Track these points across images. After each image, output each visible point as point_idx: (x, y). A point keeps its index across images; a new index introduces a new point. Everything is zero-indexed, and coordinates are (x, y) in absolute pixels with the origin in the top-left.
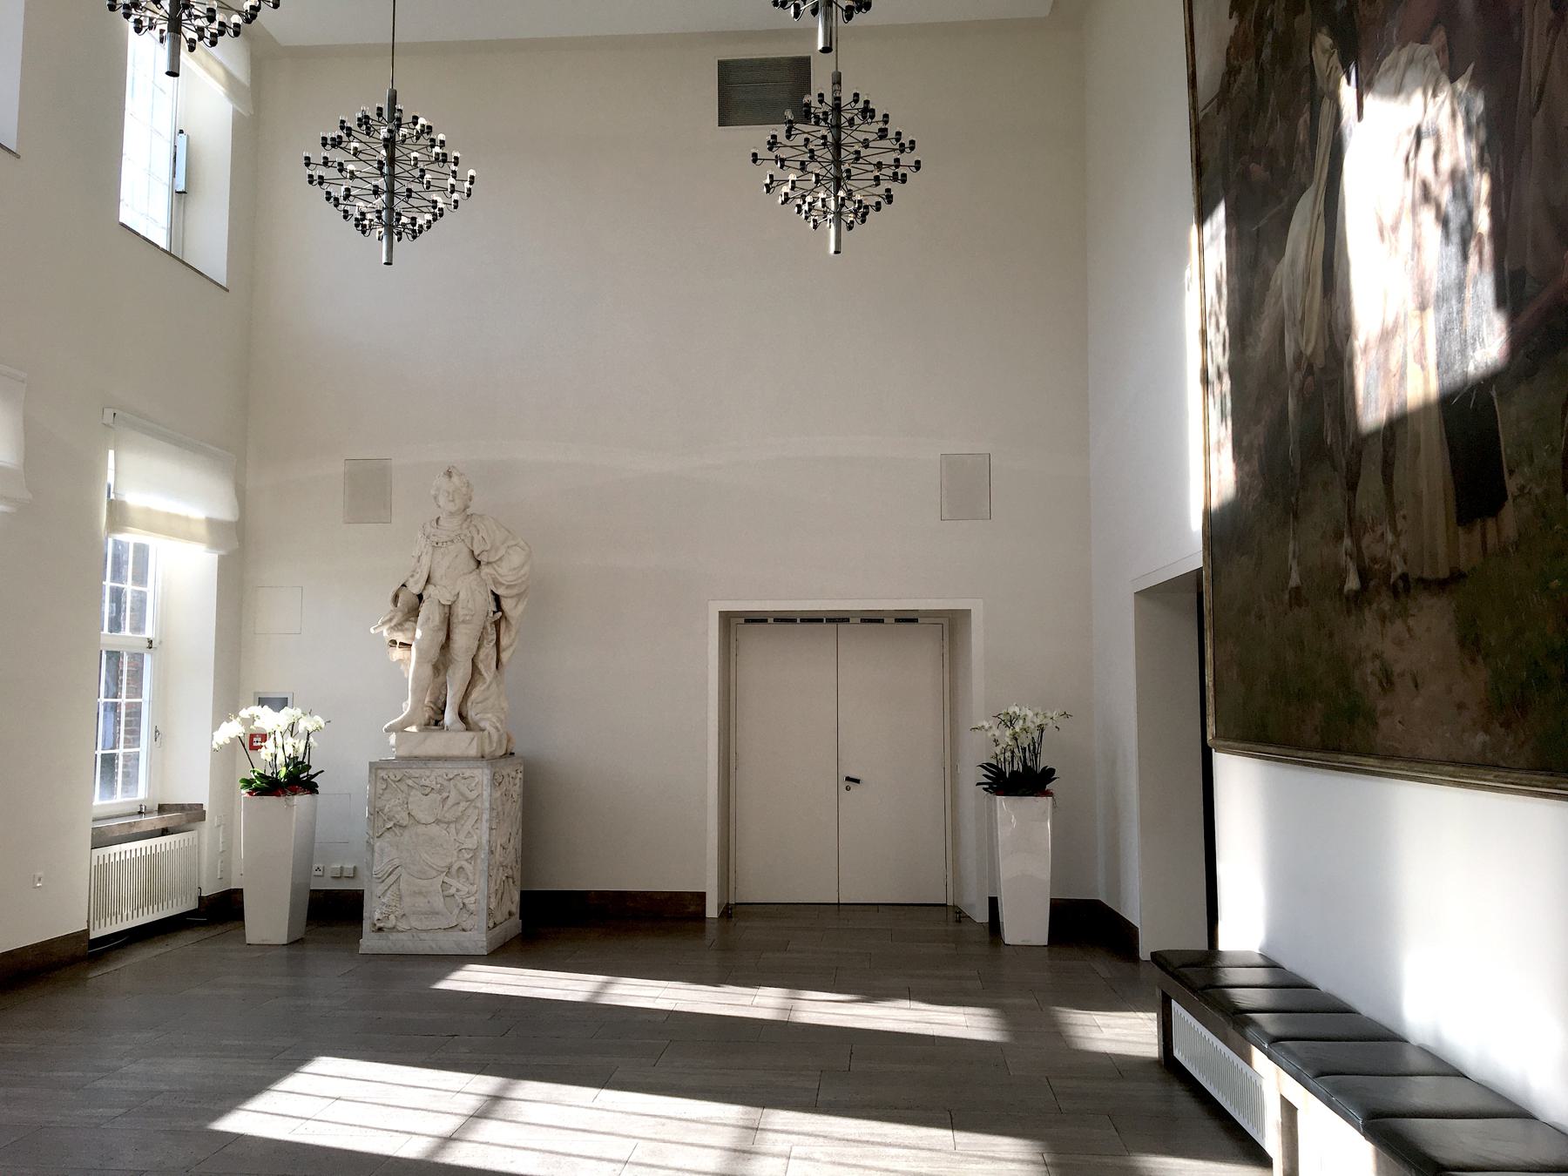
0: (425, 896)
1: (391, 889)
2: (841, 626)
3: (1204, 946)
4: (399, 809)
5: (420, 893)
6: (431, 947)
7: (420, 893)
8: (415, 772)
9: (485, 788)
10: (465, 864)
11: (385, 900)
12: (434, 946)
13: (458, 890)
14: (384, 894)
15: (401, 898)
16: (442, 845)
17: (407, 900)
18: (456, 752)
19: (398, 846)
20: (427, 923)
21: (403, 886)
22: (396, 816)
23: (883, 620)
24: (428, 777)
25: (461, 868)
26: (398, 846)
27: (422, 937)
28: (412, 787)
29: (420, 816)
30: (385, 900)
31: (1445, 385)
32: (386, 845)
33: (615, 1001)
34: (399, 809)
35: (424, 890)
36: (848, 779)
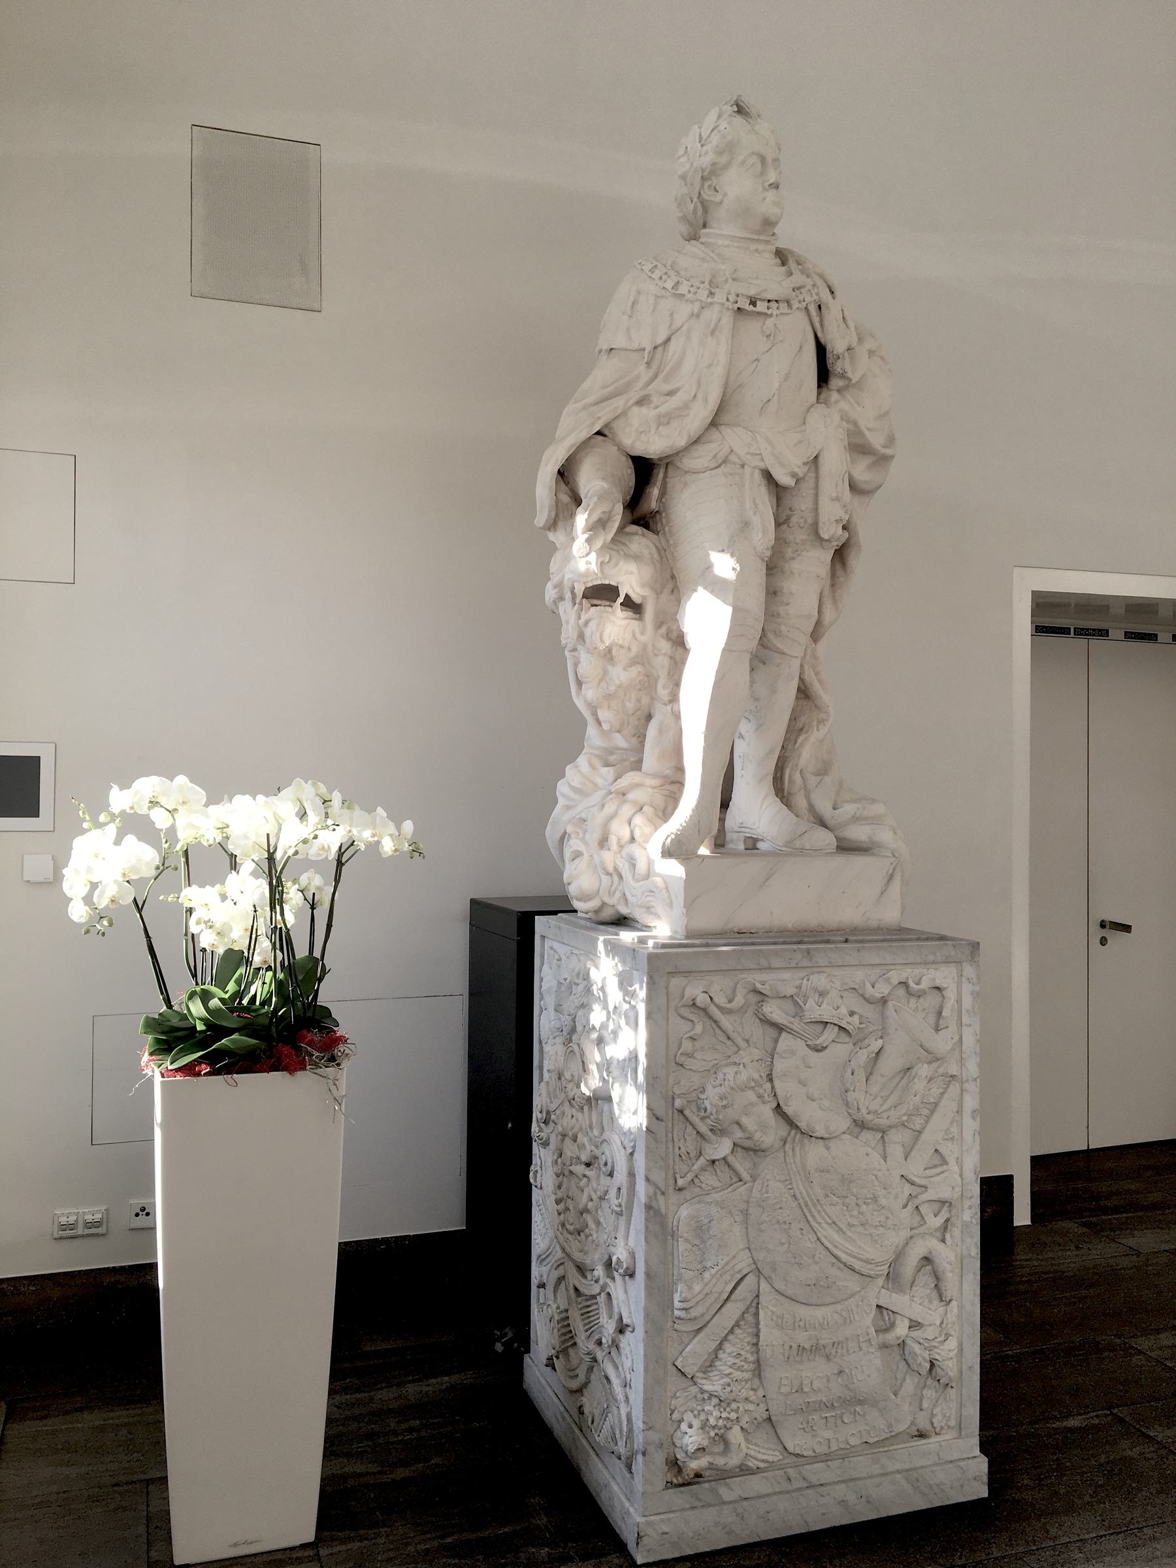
0: (828, 1358)
1: (728, 1347)
2: (1096, 643)
3: (50, 876)
4: (751, 1096)
5: (816, 1349)
6: (843, 1503)
7: (816, 1349)
8: (784, 981)
9: (965, 1020)
10: (934, 1244)
11: (713, 1385)
12: (852, 1498)
13: (915, 1325)
14: (709, 1366)
15: (758, 1369)
16: (875, 1199)
17: (779, 1376)
18: (847, 914)
19: (746, 1213)
20: (828, 1434)
21: (769, 1335)
22: (744, 1120)
23: (1156, 635)
24: (822, 994)
25: (927, 1260)
26: (746, 1213)
27: (814, 1480)
28: (780, 1028)
29: (806, 1113)
30: (713, 1385)
31: (692, 434)
32: (714, 1210)
33: (541, 1306)
34: (751, 1096)
35: (826, 1338)
36: (1103, 925)
